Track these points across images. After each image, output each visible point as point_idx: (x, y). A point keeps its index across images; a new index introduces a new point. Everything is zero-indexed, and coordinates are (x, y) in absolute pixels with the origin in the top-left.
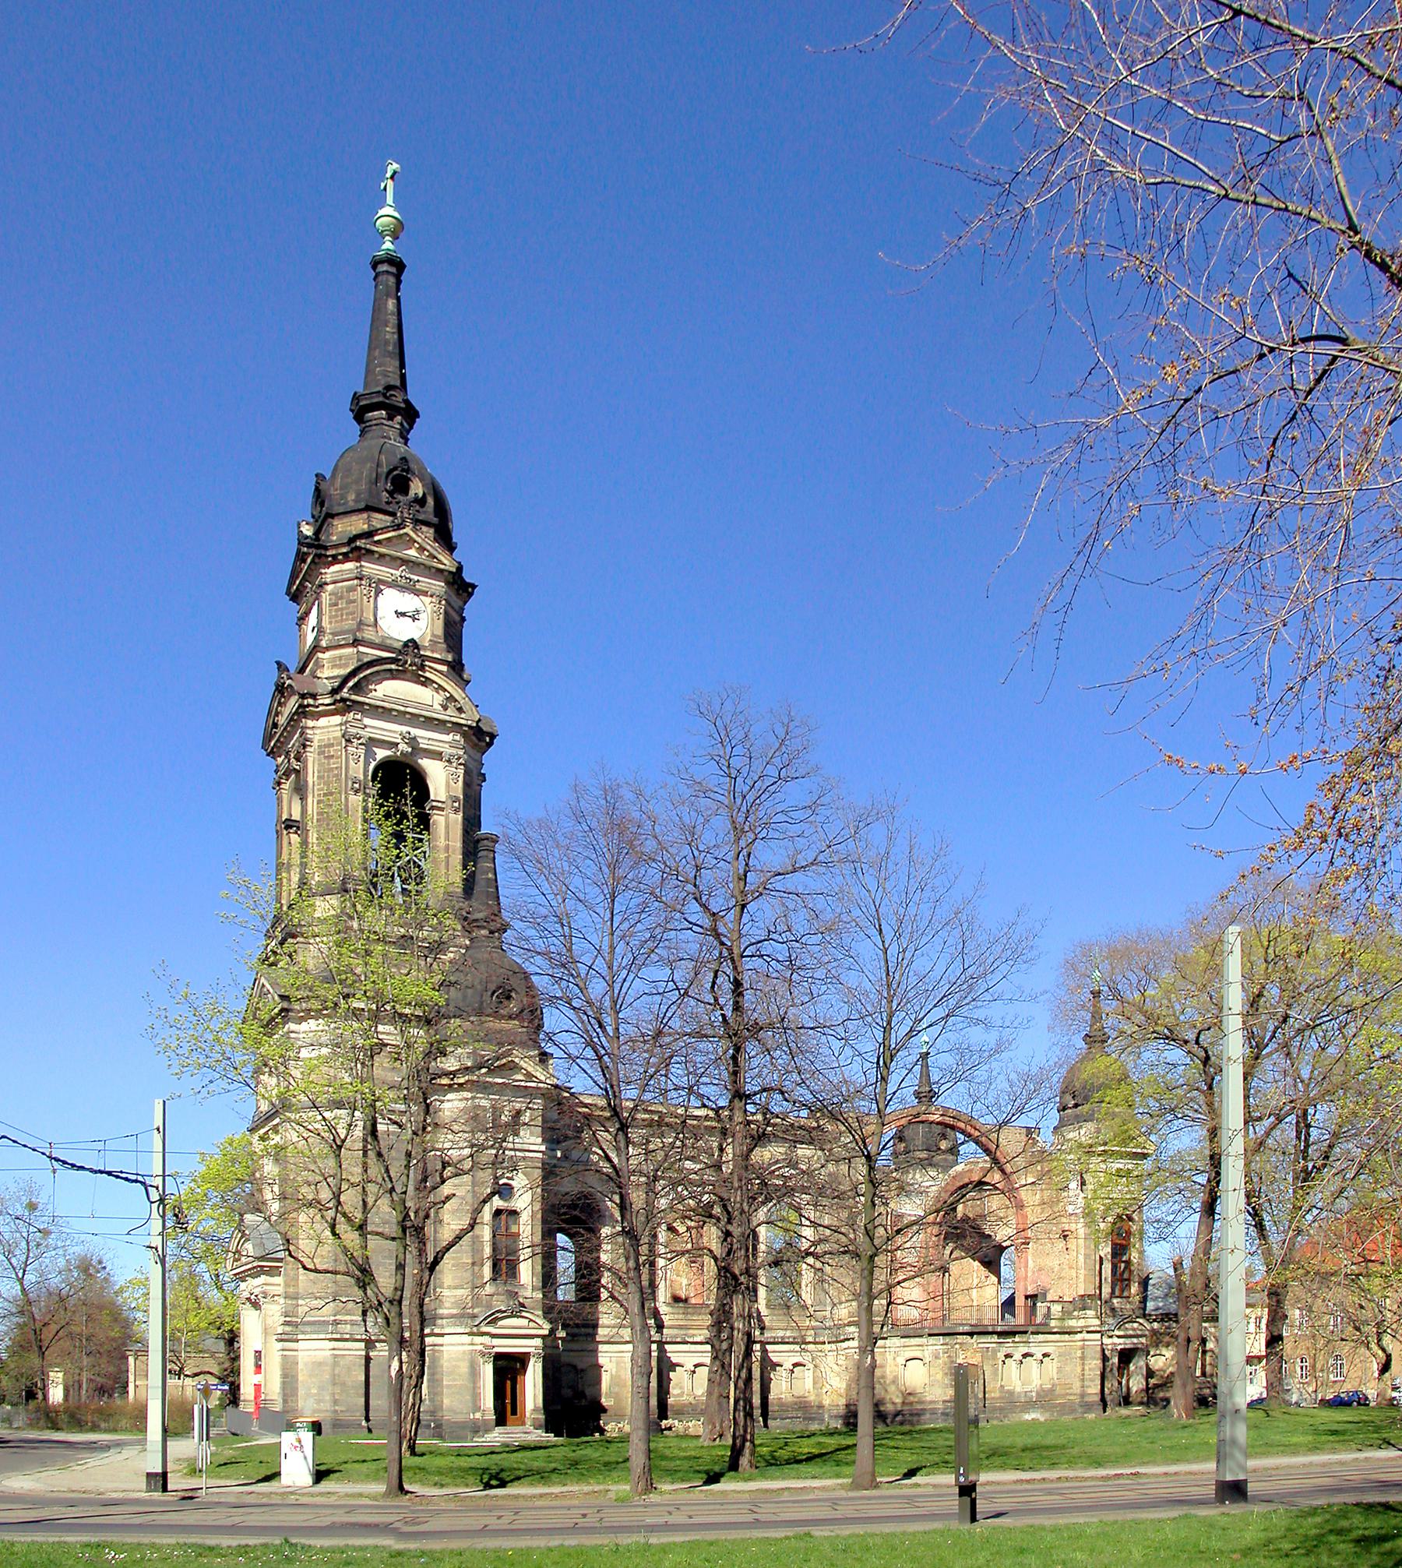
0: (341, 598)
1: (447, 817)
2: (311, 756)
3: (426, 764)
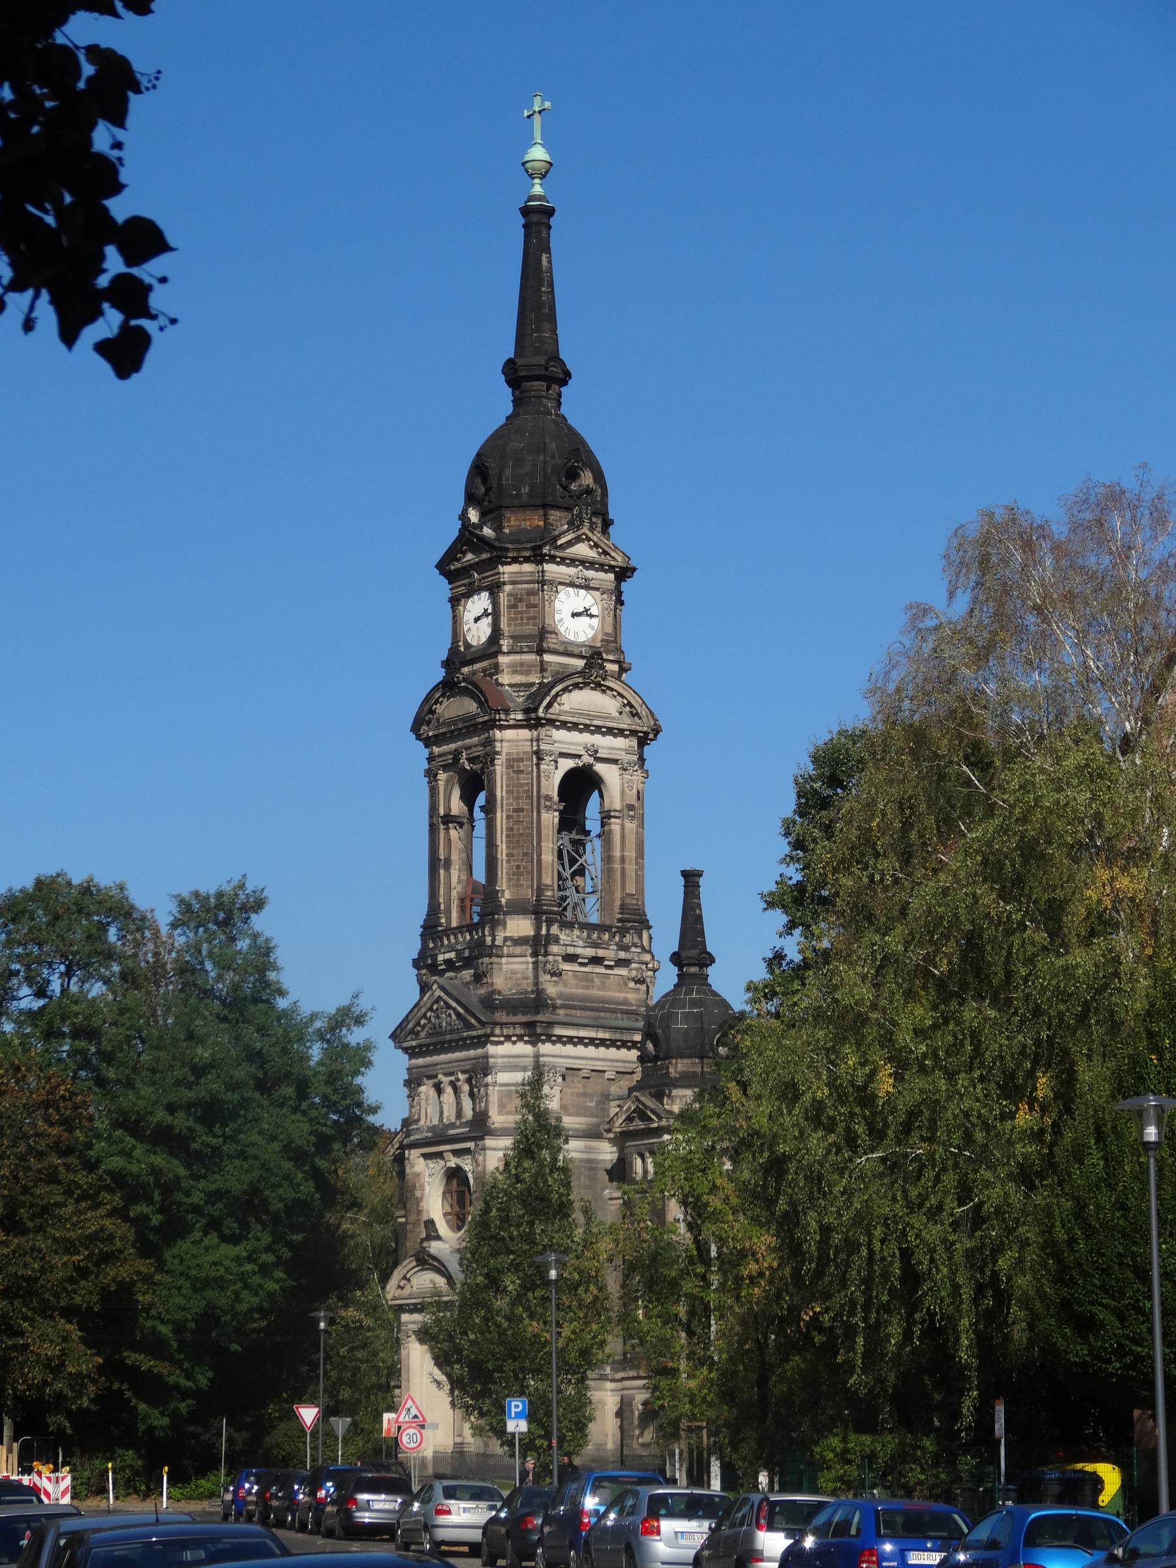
0: (521, 600)
1: (623, 826)
2: (500, 761)
3: (599, 768)
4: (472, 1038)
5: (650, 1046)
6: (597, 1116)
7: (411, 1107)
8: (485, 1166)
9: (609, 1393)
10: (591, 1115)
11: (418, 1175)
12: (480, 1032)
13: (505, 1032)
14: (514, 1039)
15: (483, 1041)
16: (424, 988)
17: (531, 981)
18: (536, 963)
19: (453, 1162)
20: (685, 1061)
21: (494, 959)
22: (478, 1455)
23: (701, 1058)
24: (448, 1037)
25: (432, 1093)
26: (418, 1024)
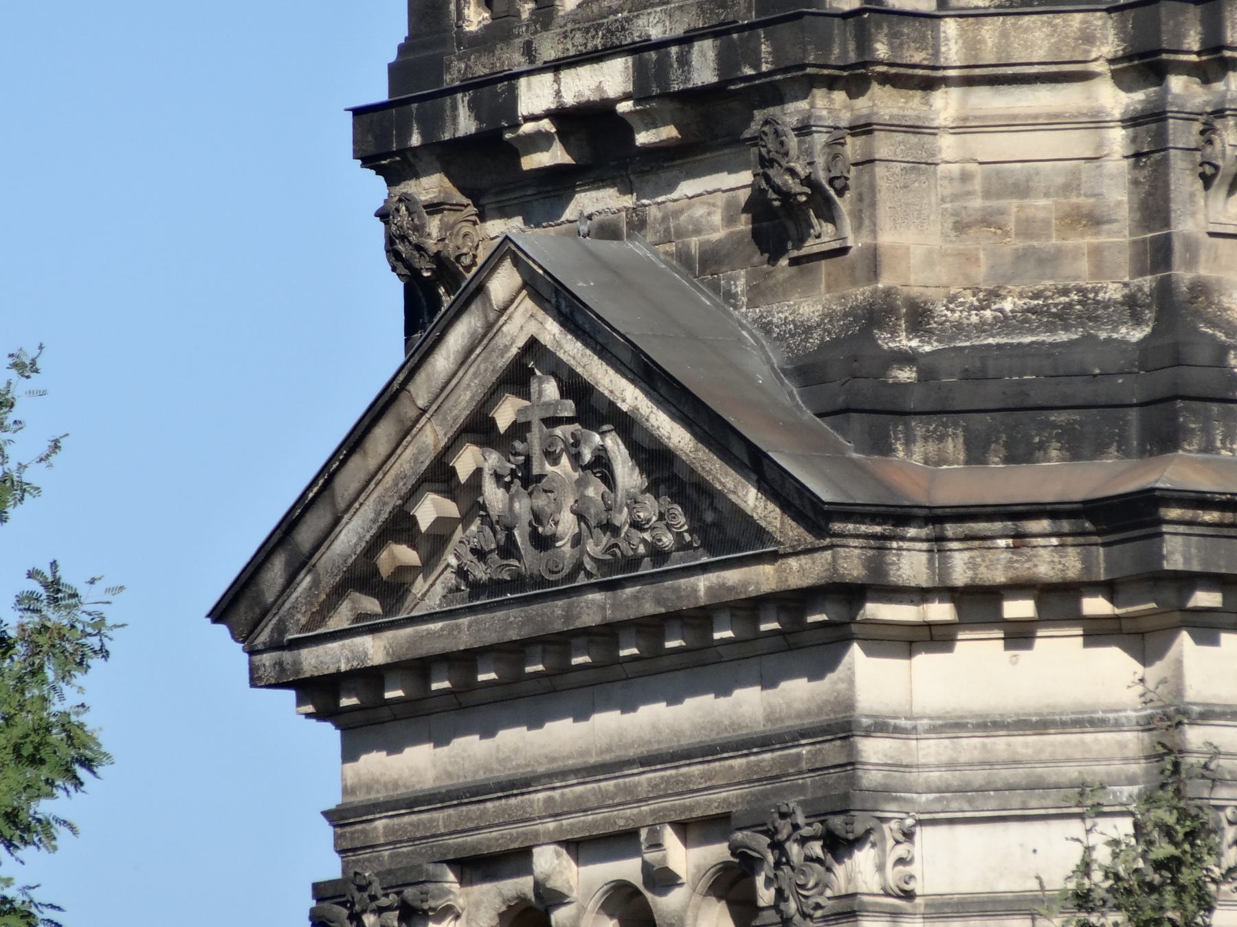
4: (754, 606)
12: (801, 572)
13: (962, 566)
14: (1019, 608)
15: (813, 628)
16: (434, 287)
17: (1120, 235)
18: (1149, 123)
21: (883, 102)
24: (593, 608)
26: (400, 525)
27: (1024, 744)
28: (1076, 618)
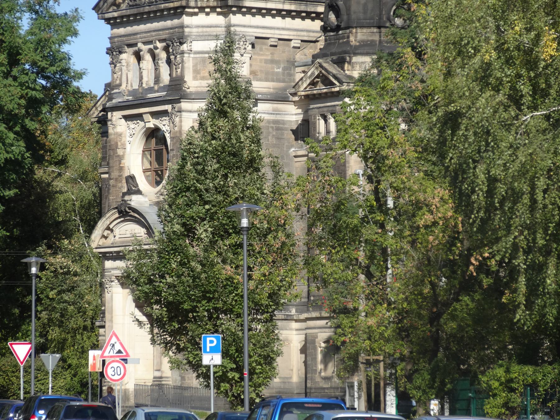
5: (332, 17)
6: (284, 81)
7: (114, 73)
8: (181, 126)
9: (295, 332)
10: (278, 81)
11: (120, 135)
14: (208, 10)
19: (152, 123)
20: (365, 30)
22: (175, 388)
23: (379, 27)
24: (147, 9)
25: (133, 60)
27: (208, 29)
28: (215, 11)
